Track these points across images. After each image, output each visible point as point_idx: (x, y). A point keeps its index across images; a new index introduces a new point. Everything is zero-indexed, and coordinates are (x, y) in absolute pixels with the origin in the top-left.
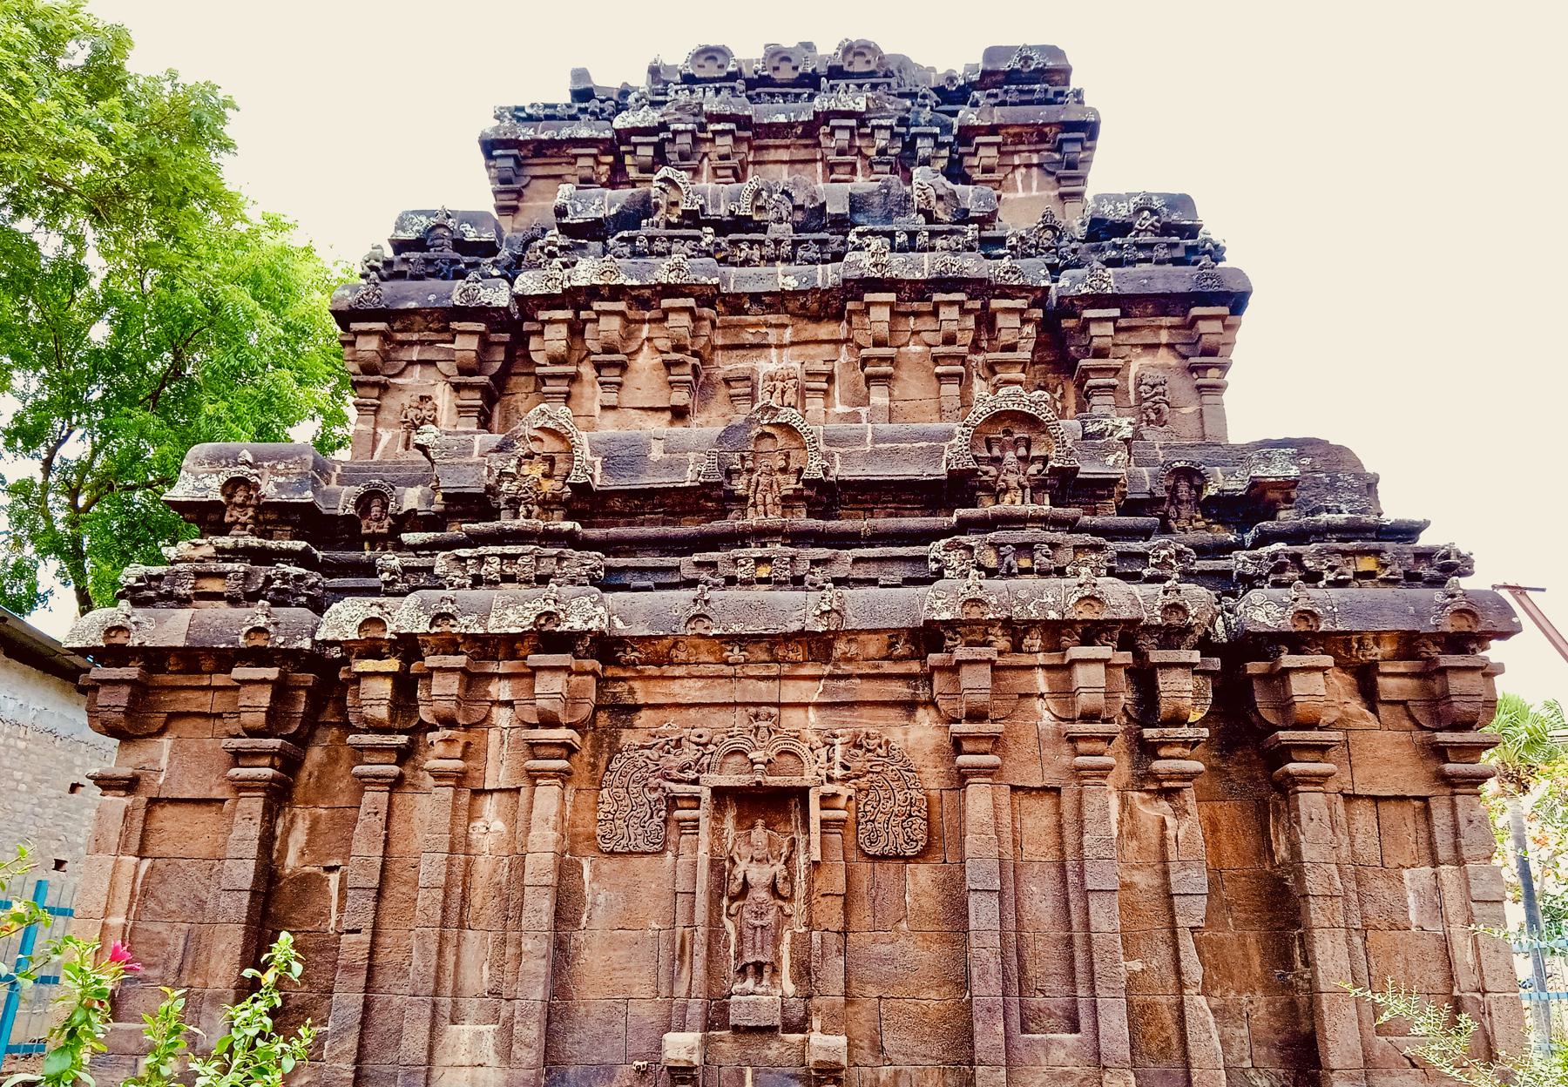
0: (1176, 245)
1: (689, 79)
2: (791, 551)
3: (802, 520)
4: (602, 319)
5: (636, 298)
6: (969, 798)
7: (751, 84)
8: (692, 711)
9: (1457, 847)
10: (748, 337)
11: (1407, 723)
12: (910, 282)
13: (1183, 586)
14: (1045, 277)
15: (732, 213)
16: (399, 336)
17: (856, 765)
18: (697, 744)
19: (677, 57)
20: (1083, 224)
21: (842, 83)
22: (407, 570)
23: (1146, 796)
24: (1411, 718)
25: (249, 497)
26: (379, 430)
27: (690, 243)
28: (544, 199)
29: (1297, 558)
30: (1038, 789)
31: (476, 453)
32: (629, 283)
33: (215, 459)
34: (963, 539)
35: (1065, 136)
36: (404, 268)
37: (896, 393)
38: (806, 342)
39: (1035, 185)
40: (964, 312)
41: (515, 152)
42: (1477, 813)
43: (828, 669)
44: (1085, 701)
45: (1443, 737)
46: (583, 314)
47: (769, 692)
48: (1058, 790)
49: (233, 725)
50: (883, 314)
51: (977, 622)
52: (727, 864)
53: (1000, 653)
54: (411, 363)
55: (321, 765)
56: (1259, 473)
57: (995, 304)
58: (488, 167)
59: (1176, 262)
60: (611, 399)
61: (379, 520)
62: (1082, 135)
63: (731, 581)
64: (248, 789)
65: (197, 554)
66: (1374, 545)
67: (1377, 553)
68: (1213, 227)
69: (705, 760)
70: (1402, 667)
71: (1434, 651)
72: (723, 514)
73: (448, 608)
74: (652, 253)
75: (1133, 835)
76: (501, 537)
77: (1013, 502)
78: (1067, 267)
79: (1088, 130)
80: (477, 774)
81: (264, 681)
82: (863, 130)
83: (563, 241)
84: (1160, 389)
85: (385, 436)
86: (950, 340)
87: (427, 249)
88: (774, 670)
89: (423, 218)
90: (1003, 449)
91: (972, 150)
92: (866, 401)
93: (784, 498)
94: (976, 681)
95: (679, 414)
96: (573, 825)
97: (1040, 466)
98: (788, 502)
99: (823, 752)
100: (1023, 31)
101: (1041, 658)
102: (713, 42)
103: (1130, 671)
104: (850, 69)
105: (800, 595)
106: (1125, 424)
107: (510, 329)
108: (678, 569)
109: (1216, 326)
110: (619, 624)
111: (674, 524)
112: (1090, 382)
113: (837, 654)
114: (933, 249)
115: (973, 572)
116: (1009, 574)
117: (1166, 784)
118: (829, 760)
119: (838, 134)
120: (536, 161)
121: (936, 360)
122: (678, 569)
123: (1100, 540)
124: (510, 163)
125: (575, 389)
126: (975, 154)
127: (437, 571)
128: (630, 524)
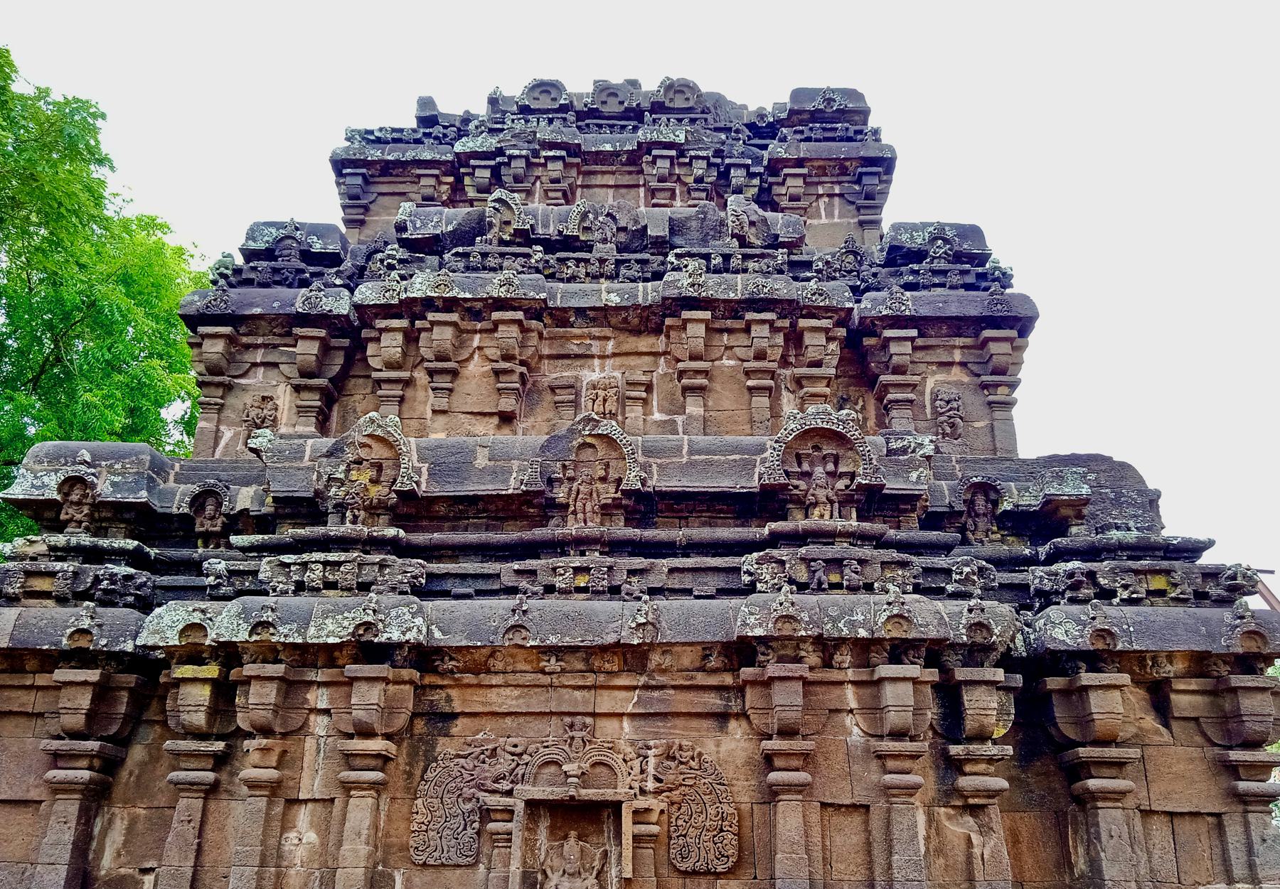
0: (967, 272)
1: (525, 110)
2: (609, 560)
3: (620, 529)
4: (436, 329)
5: (469, 310)
6: (779, 816)
7: (580, 116)
8: (508, 720)
9: (1251, 866)
10: (573, 348)
11: (1199, 739)
12: (725, 301)
13: (986, 604)
14: (849, 300)
15: (560, 233)
16: (245, 340)
17: (669, 777)
18: (513, 754)
19: (514, 89)
20: (882, 250)
21: (664, 118)
22: (232, 573)
23: (951, 811)
24: (1204, 735)
25: (85, 496)
26: (222, 428)
27: (521, 260)
28: (389, 215)
29: (1091, 575)
30: (847, 806)
31: (307, 458)
32: (462, 295)
33: (54, 459)
34: (775, 553)
35: (864, 170)
36: (252, 275)
37: (710, 403)
38: (627, 354)
39: (836, 212)
40: (774, 330)
41: (364, 171)
42: (1271, 832)
43: (642, 680)
44: (894, 719)
45: (1236, 755)
46: (418, 324)
47: (585, 702)
48: (867, 808)
49: (53, 726)
50: (700, 330)
51: (790, 638)
52: (540, 877)
53: (811, 669)
54: (255, 365)
55: (143, 765)
56: (1053, 491)
57: (803, 323)
58: (338, 184)
59: (968, 287)
60: (443, 403)
61: (212, 518)
62: (880, 169)
63: (550, 589)
64: (65, 791)
65: (31, 551)
66: (1165, 564)
67: (1167, 572)
68: (1002, 252)
69: (520, 771)
70: (1194, 684)
71: (1224, 670)
72: (543, 521)
73: (268, 616)
74: (484, 268)
75: (939, 852)
76: (325, 544)
77: (822, 516)
78: (868, 289)
79: (883, 165)
80: (291, 783)
81: (85, 683)
82: (682, 160)
83: (402, 254)
84: (955, 405)
85: (227, 434)
86: (760, 356)
87: (275, 259)
88: (590, 679)
89: (273, 231)
90: (812, 464)
91: (780, 180)
92: (682, 410)
93: (604, 507)
94: (788, 698)
95: (506, 419)
96: (387, 835)
97: (848, 482)
98: (606, 511)
99: (636, 764)
100: (826, 74)
101: (850, 674)
102: (546, 77)
103: (936, 687)
104: (671, 105)
105: (616, 605)
106: (927, 441)
107: (349, 334)
108: (498, 576)
109: (1005, 347)
110: (437, 634)
111: (495, 529)
112: (890, 396)
113: (652, 665)
114: (745, 271)
115: (786, 588)
116: (820, 589)
117: (971, 801)
118: (642, 772)
119: (659, 163)
120: (382, 179)
121: (748, 374)
122: (498, 576)
123: (905, 556)
124: (359, 180)
125: (409, 393)
126: (783, 184)
127: (261, 576)
128: (454, 529)
